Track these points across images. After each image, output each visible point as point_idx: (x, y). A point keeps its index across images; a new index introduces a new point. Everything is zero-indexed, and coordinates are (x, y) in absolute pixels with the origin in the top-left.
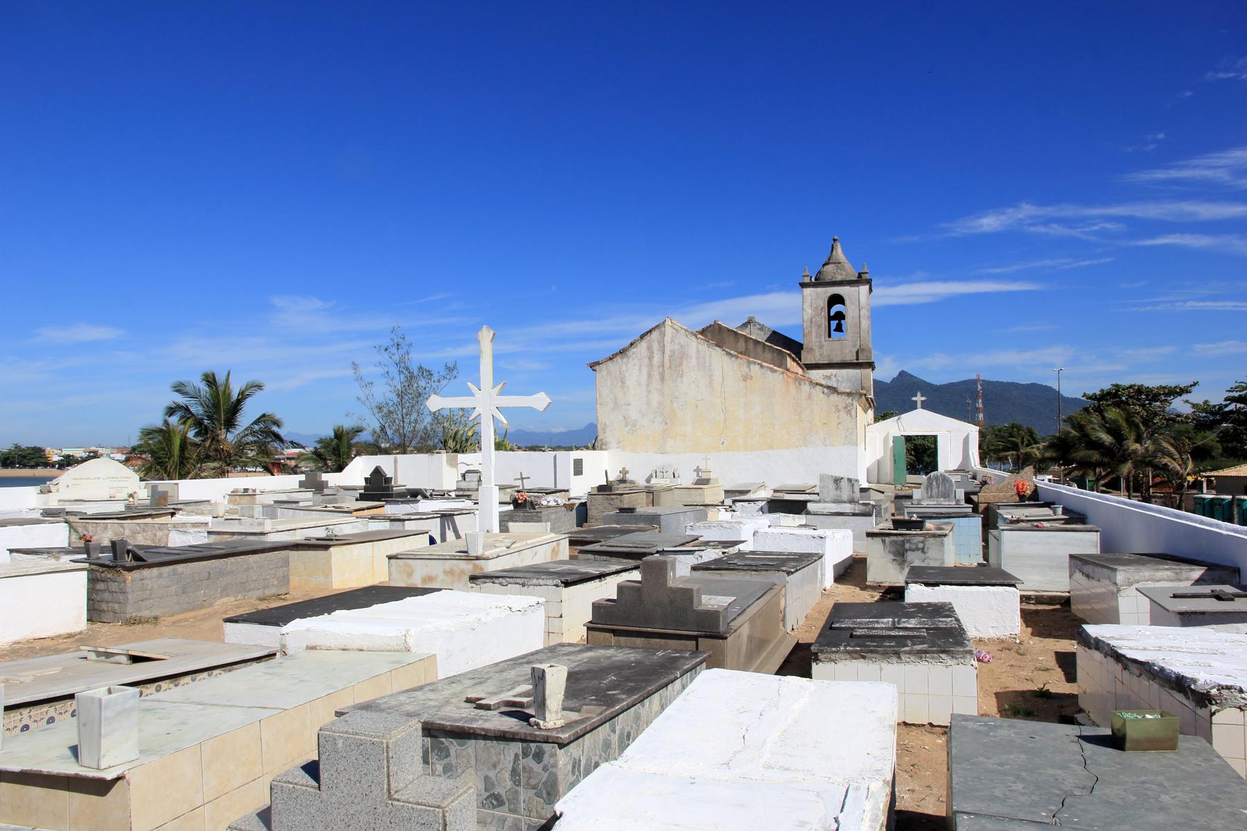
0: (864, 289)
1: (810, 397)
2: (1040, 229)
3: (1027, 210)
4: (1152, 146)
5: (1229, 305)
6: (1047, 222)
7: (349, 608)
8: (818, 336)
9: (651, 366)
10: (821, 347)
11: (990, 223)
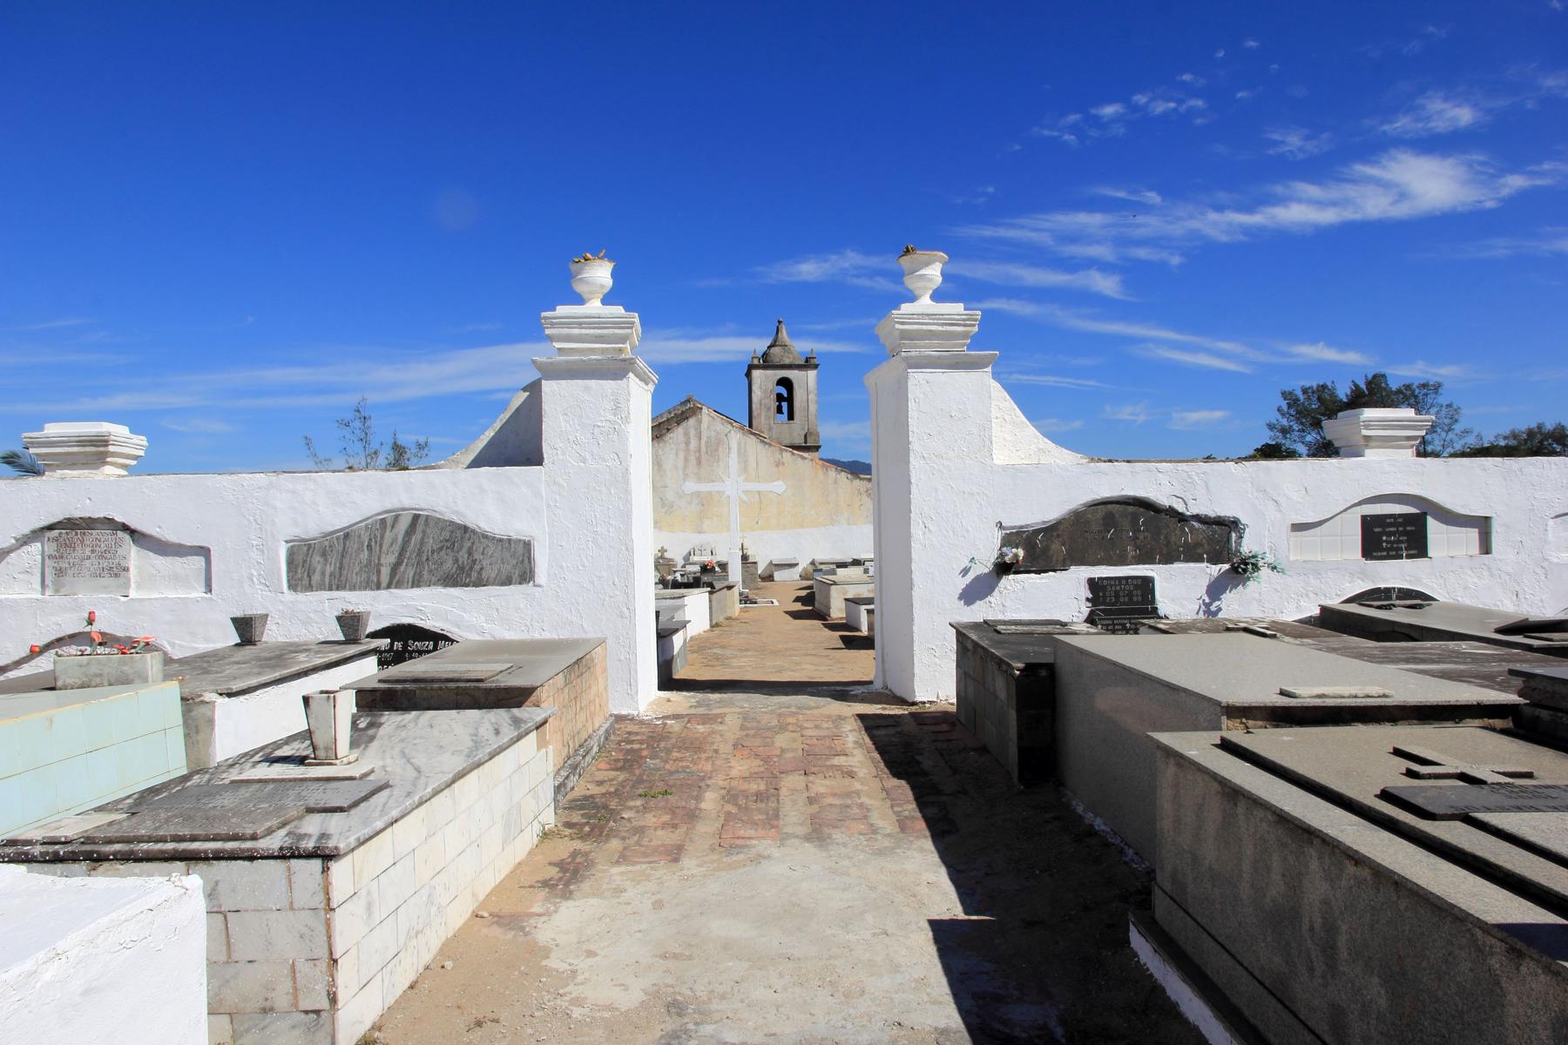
0: (812, 374)
1: (835, 482)
2: (864, 282)
3: (852, 259)
4: (982, 200)
5: (1049, 380)
6: (874, 273)
7: (910, 585)
8: (768, 418)
9: (687, 450)
10: (770, 429)
11: (809, 270)
